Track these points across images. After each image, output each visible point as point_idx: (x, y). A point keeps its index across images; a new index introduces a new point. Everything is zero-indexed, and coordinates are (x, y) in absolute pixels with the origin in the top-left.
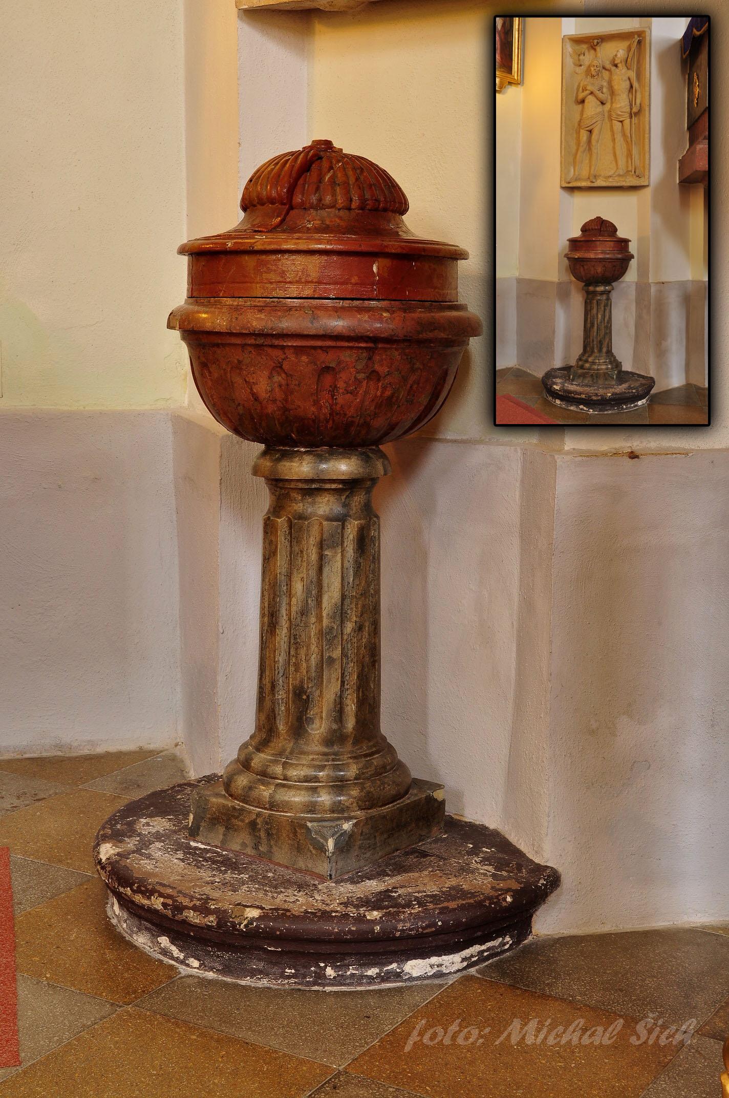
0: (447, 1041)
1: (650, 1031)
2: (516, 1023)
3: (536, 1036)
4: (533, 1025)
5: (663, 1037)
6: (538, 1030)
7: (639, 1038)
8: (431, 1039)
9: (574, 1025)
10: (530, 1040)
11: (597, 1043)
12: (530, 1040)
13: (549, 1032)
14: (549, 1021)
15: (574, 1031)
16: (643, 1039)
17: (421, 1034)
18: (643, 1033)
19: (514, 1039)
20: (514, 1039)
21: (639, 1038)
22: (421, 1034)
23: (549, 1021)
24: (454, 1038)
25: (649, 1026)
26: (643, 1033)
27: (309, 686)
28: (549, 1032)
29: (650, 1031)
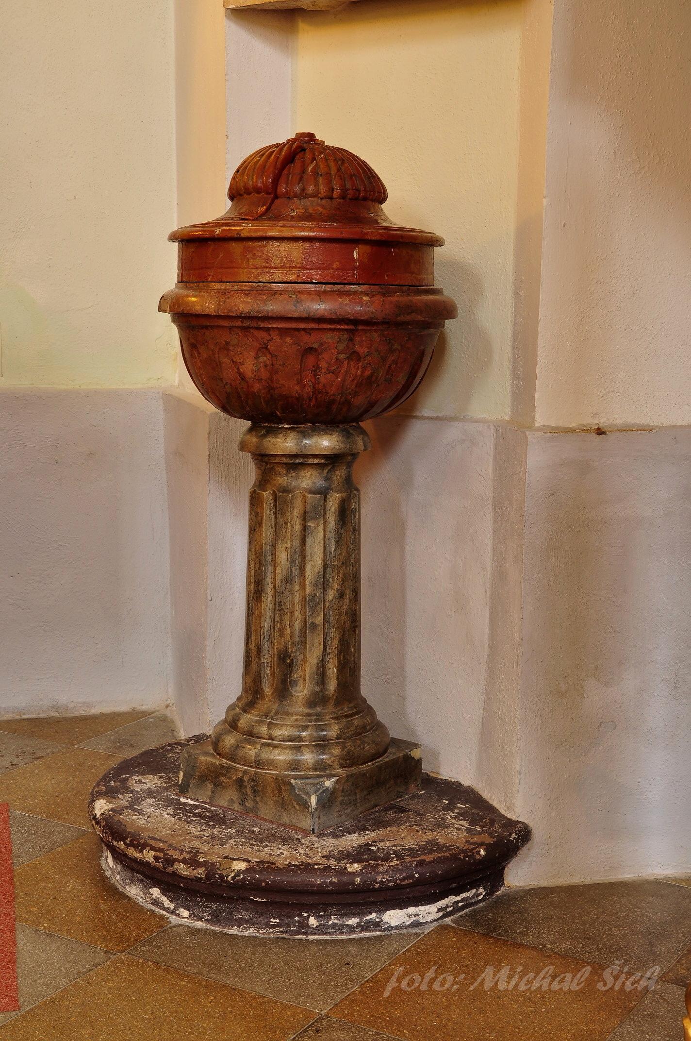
0: (424, 987)
1: (616, 978)
2: (490, 970)
3: (508, 982)
4: (505, 971)
5: (629, 983)
6: (510, 977)
7: (605, 984)
8: (409, 985)
9: (544, 972)
10: (502, 986)
11: (565, 989)
12: (502, 986)
13: (520, 979)
14: (521, 968)
15: (544, 978)
16: (609, 985)
17: (399, 980)
18: (610, 980)
19: (488, 985)
20: (488, 985)
21: (605, 985)
22: (399, 980)
23: (521, 968)
24: (430, 984)
25: (615, 973)
26: (610, 980)
27: (293, 650)
28: (520, 979)
29: (616, 978)
